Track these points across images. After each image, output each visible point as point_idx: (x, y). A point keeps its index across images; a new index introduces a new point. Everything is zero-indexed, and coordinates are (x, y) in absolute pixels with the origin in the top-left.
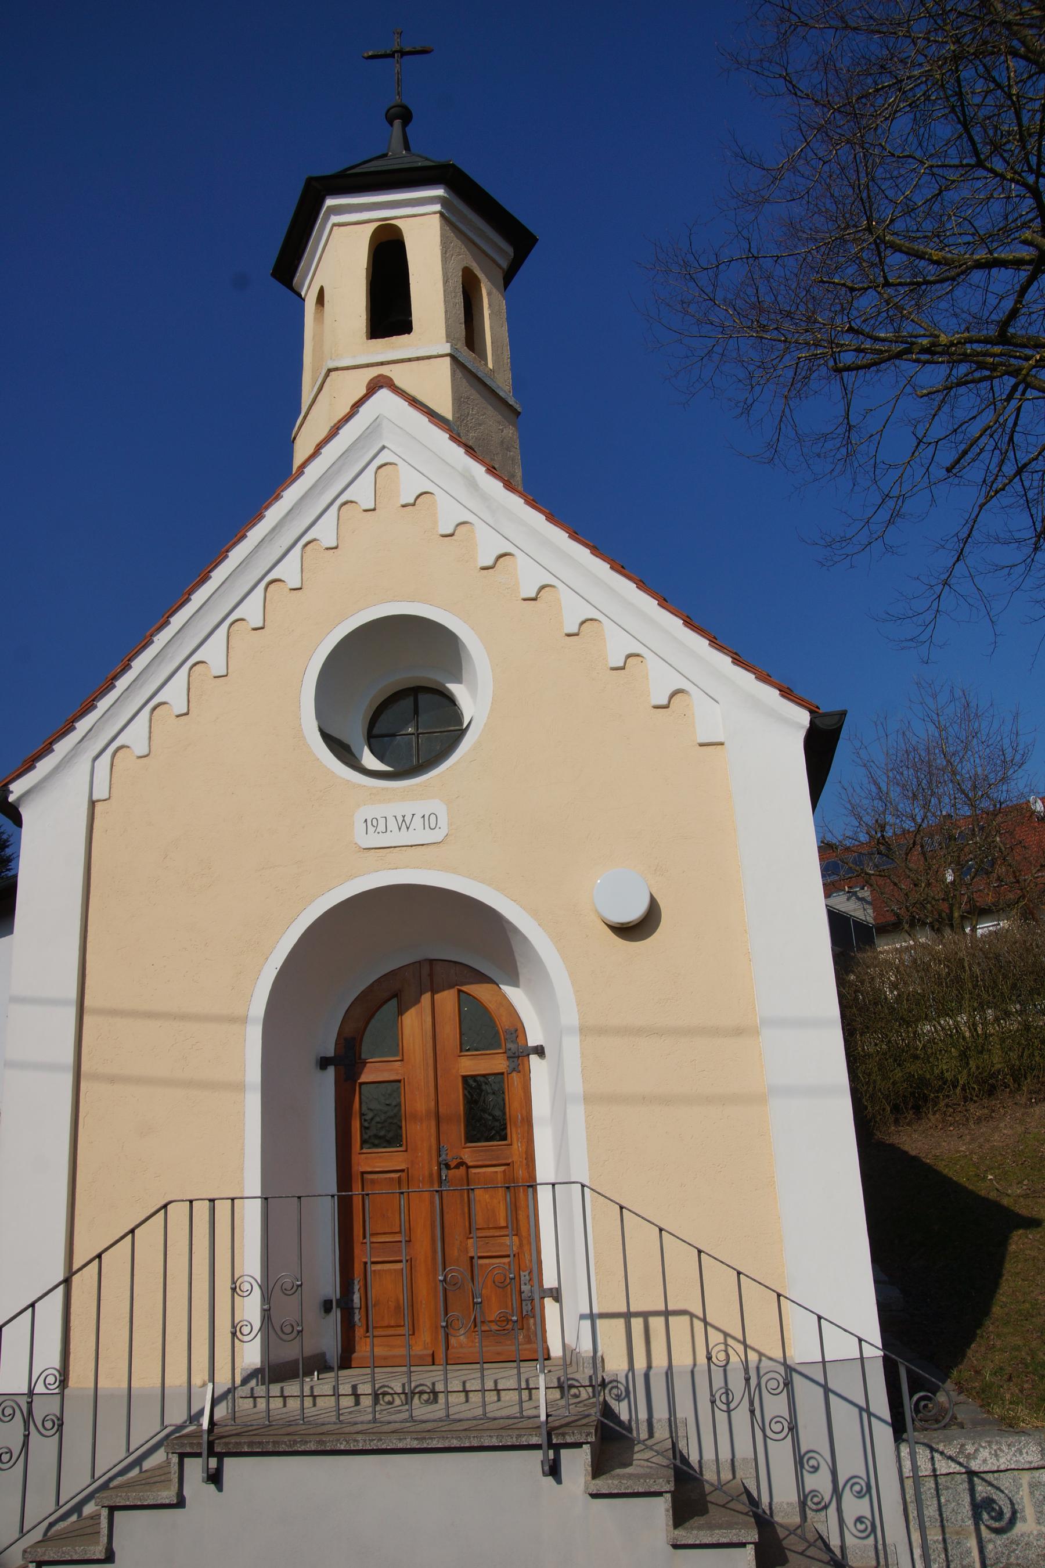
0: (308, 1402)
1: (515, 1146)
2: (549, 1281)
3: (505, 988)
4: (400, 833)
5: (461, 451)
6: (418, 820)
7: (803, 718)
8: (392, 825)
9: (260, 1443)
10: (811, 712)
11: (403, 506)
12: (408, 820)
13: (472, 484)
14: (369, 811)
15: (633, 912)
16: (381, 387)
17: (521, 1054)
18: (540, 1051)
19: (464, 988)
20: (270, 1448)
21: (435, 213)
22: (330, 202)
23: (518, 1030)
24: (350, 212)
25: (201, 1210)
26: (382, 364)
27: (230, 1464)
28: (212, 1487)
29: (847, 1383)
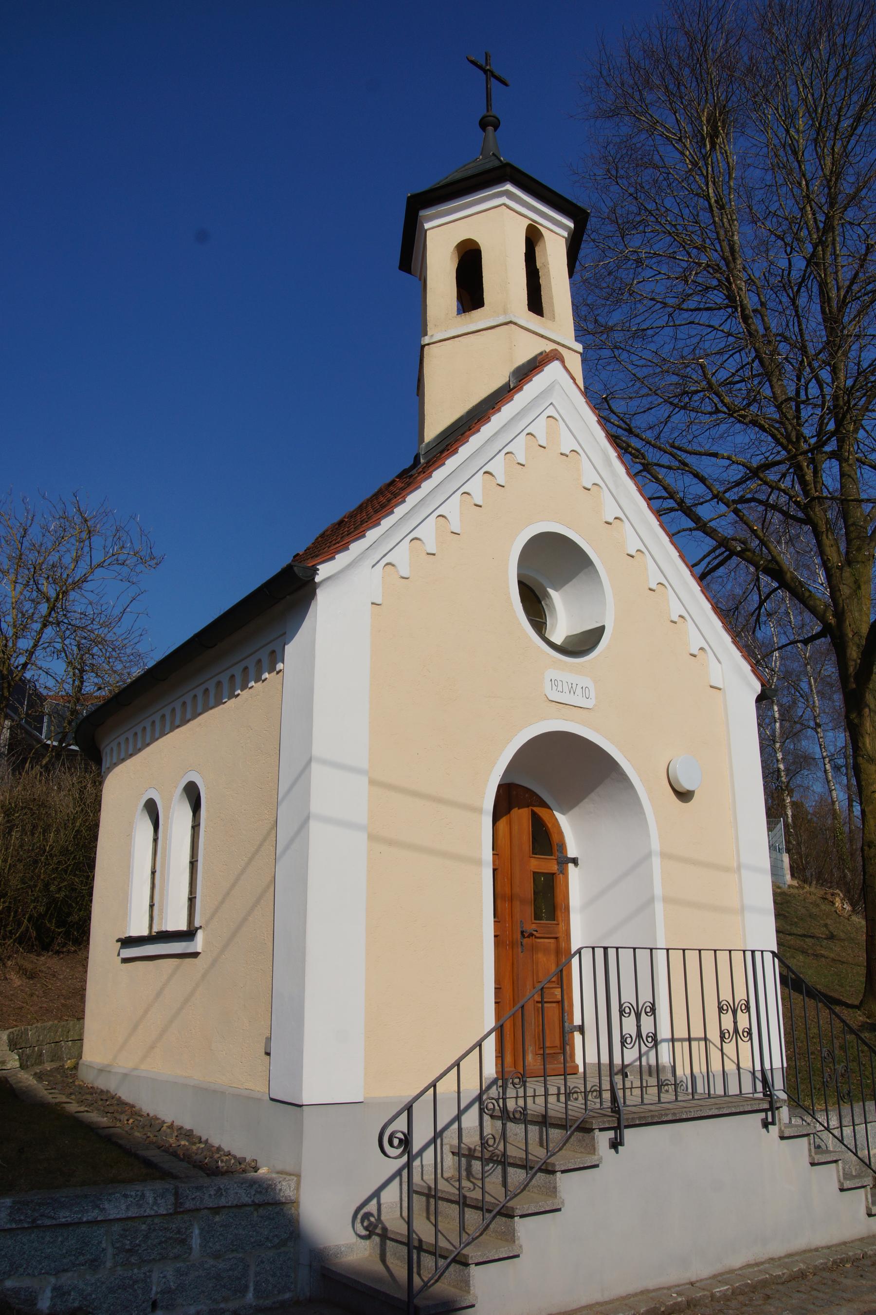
1: (560, 926)
2: (577, 1021)
6: (579, 687)
7: (758, 688)
8: (566, 689)
9: (645, 1117)
10: (763, 685)
11: (562, 454)
12: (574, 686)
14: (551, 674)
15: (686, 785)
16: (557, 359)
18: (575, 861)
19: (535, 809)
20: (650, 1120)
21: (563, 237)
22: (509, 187)
23: (562, 846)
24: (517, 202)
25: (599, 953)
26: (563, 346)
27: (628, 1134)
28: (613, 1150)
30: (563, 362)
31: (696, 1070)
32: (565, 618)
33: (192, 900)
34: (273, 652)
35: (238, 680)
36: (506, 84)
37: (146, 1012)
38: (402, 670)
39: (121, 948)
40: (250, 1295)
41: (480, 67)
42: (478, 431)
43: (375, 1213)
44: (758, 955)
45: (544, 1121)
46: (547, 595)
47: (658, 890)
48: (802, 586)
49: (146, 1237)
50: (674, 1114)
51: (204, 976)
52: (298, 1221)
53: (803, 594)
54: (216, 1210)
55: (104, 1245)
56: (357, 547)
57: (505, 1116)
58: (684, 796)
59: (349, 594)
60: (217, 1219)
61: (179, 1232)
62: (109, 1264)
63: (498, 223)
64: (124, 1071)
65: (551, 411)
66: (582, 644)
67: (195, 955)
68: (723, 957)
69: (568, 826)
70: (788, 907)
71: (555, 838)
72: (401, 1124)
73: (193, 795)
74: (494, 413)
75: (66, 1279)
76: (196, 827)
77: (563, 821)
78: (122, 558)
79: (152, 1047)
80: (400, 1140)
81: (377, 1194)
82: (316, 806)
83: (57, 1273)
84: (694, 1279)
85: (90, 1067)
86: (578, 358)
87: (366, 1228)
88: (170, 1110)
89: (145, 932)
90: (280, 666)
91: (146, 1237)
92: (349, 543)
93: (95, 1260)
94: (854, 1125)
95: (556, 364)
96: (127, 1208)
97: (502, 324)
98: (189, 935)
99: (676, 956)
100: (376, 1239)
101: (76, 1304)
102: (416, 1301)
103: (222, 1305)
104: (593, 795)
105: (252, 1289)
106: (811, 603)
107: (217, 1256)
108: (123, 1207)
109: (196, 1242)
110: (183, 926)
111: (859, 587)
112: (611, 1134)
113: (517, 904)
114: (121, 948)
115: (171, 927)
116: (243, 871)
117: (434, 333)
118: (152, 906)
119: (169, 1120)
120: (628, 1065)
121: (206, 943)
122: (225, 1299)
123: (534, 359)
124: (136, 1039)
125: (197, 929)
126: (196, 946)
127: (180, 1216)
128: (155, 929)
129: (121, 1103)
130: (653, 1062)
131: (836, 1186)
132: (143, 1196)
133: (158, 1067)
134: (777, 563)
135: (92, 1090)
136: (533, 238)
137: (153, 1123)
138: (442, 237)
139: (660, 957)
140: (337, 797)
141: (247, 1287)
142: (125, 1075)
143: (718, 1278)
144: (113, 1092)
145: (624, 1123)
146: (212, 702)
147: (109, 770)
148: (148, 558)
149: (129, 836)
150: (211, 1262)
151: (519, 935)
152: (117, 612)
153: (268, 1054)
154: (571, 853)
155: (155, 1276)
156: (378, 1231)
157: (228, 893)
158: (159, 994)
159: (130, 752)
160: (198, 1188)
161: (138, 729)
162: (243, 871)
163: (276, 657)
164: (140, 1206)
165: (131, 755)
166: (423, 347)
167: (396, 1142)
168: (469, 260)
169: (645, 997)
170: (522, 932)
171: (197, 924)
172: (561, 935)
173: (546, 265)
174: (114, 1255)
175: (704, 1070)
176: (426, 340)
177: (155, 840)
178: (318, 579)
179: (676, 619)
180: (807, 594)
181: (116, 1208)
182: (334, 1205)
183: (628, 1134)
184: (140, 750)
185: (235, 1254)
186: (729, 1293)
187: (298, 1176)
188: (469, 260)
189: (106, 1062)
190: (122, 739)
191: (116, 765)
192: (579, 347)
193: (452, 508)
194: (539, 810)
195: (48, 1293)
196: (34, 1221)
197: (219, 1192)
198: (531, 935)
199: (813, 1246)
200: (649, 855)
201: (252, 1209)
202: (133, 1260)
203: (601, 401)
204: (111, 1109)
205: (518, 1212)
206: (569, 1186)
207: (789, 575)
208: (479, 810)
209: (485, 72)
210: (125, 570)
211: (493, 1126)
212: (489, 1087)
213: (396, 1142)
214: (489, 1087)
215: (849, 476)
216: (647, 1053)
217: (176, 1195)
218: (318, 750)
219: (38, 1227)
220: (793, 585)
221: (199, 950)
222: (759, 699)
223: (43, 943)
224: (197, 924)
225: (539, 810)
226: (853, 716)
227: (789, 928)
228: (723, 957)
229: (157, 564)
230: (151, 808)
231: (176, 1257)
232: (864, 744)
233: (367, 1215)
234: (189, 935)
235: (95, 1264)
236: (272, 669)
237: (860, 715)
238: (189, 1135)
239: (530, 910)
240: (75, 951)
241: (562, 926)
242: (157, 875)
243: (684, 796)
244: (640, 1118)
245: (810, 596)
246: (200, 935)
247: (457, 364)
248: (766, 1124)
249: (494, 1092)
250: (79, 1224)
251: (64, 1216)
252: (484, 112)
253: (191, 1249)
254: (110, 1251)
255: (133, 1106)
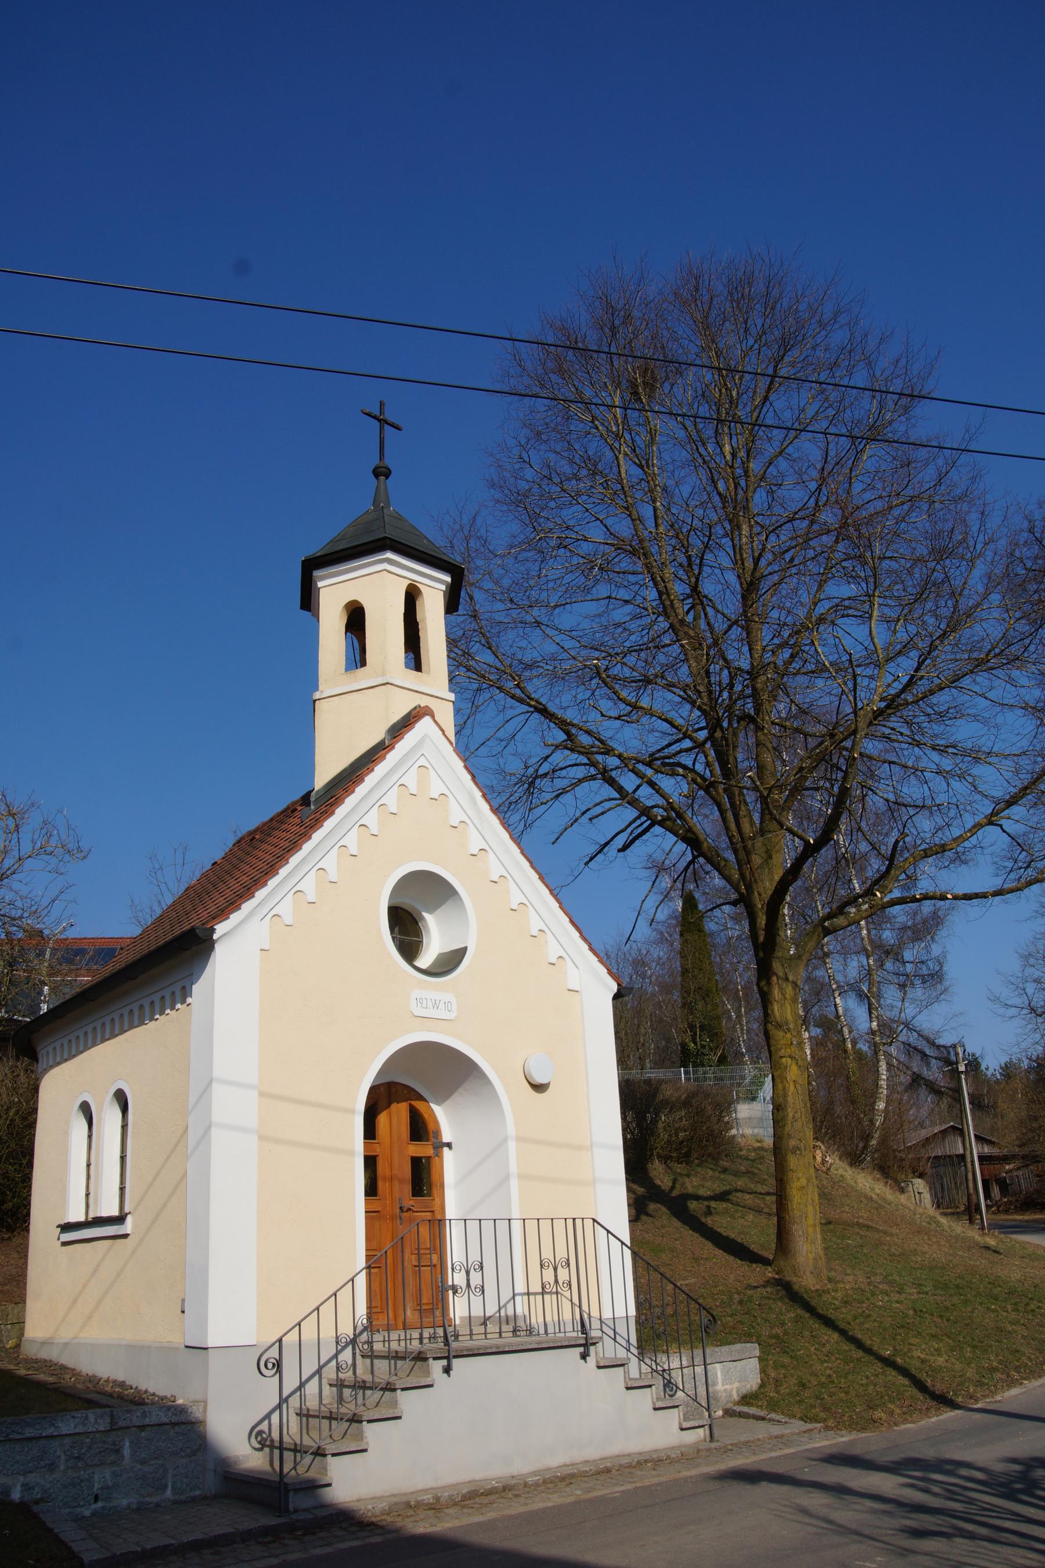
0: (402, 1337)
3: (433, 1106)
4: (426, 1011)
5: (469, 777)
6: (442, 1003)
7: (614, 987)
8: (430, 1005)
10: (619, 985)
13: (473, 800)
14: (416, 993)
15: (540, 1079)
17: (440, 1146)
18: (449, 1145)
19: (413, 1103)
23: (438, 1133)
27: (455, 1362)
29: (621, 1329)
30: (433, 717)
31: (548, 1319)
32: (437, 936)
33: (122, 1189)
34: (184, 987)
35: (157, 1006)
36: (398, 428)
37: (84, 1287)
38: (285, 1006)
39: (61, 1232)
40: (169, 1492)
41: (375, 417)
42: (353, 792)
43: (267, 1431)
44: (579, 1222)
45: (397, 1356)
46: (422, 918)
47: (513, 1168)
48: (718, 856)
49: (90, 1448)
50: (498, 1347)
51: (133, 1253)
52: (205, 1437)
53: (719, 864)
54: (142, 1428)
55: (58, 1453)
56: (247, 907)
57: (371, 1356)
58: (539, 1088)
59: (242, 942)
60: (143, 1434)
61: (114, 1444)
62: (62, 1467)
63: (379, 585)
64: (64, 1341)
65: (422, 762)
66: (450, 962)
67: (125, 1236)
68: (545, 1225)
69: (444, 1116)
70: (761, 1163)
71: (431, 1127)
72: (274, 1353)
73: (121, 1099)
74: (368, 774)
75: (31, 1478)
76: (124, 1127)
77: (440, 1112)
78: (49, 849)
79: (90, 1318)
80: (274, 1364)
81: (268, 1416)
82: (216, 1116)
83: (25, 1473)
84: (515, 1474)
85: (32, 1341)
86: (450, 708)
87: (259, 1443)
88: (107, 1369)
89: (82, 1218)
90: (189, 1000)
91: (90, 1448)
92: (240, 904)
93: (52, 1464)
94: (705, 1365)
95: (427, 719)
96: (75, 1427)
97: (383, 685)
98: (120, 1219)
99: (532, 1226)
100: (267, 1450)
101: (39, 1496)
102: (285, 1480)
103: (148, 1499)
104: (461, 1090)
105: (170, 1487)
106: (727, 872)
107: (143, 1462)
108: (72, 1425)
109: (127, 1452)
110: (115, 1212)
111: (770, 857)
112: (445, 1362)
113: (396, 1183)
114: (61, 1232)
115: (105, 1213)
116: (163, 1166)
117: (326, 687)
118: (87, 1195)
119: (105, 1376)
120: (490, 1317)
121: (135, 1225)
122: (150, 1495)
123: (409, 714)
124: (75, 1313)
125: (127, 1215)
126: (126, 1229)
127: (114, 1433)
128: (91, 1215)
129: (64, 1368)
130: (510, 1312)
131: (651, 1406)
132: (87, 1417)
133: (96, 1333)
134: (693, 833)
135: (36, 1361)
136: (412, 596)
137: (93, 1380)
138: (335, 591)
139: (516, 1226)
140: (233, 1108)
141: (166, 1486)
142: (66, 1344)
143: (534, 1473)
144: (55, 1360)
145: (452, 1354)
146: (136, 1021)
147: (46, 1071)
148: (75, 851)
149: (66, 1133)
150: (139, 1467)
151: (398, 1210)
152: (45, 902)
153: (183, 1312)
154: (446, 1138)
155: (96, 1477)
156: (268, 1443)
157: (151, 1185)
158: (95, 1271)
159: (65, 1056)
160: (128, 1411)
161: (72, 1037)
162: (163, 1166)
163: (185, 993)
164: (85, 1425)
165: (66, 1060)
166: (315, 701)
167: (270, 1365)
168: (356, 619)
169: (474, 1257)
170: (401, 1208)
171: (127, 1210)
172: (436, 1208)
173: (424, 620)
174: (66, 1461)
175: (556, 1318)
176: (317, 695)
177: (90, 1137)
178: (215, 937)
179: (535, 933)
180: (723, 863)
181: (67, 1426)
182: (233, 1427)
183: (455, 1362)
184: (74, 1056)
185: (156, 1461)
186: (541, 1482)
187: (205, 1402)
188: (356, 619)
189: (48, 1336)
190: (58, 1044)
191: (52, 1067)
192: (452, 696)
193: (330, 862)
194: (417, 1104)
195: (19, 1488)
196: (8, 1435)
197: (144, 1414)
198: (409, 1210)
199: (626, 1452)
200: (505, 1140)
201: (169, 1427)
202: (80, 1464)
203: (466, 747)
204: (56, 1373)
205: (365, 1418)
206: (408, 1402)
207: (705, 845)
208: (353, 1111)
209: (380, 421)
210: (53, 861)
211: (363, 1363)
212: (361, 1333)
213: (270, 1365)
214: (361, 1333)
215: (764, 745)
216: (505, 1305)
217: (112, 1416)
218: (217, 1072)
219: (10, 1440)
220: (709, 854)
221: (129, 1232)
222: (616, 997)
223: (11, 1229)
224: (127, 1210)
225: (417, 1104)
226: (763, 983)
227: (752, 1186)
228: (545, 1225)
229: (84, 858)
230: (85, 1109)
231: (113, 1463)
232: (773, 1011)
233: (260, 1432)
234: (120, 1219)
235: (52, 1467)
236: (183, 1002)
237: (769, 983)
238: (122, 1384)
239: (408, 1188)
240: (9, 1239)
241: (437, 1201)
242: (92, 1167)
243: (539, 1088)
244: (468, 1350)
245: (725, 865)
246: (129, 1219)
247: (344, 721)
248: (584, 1356)
249: (364, 1337)
250: (40, 1438)
251: (29, 1432)
252: (375, 462)
253: (123, 1457)
254: (63, 1457)
255: (74, 1370)
